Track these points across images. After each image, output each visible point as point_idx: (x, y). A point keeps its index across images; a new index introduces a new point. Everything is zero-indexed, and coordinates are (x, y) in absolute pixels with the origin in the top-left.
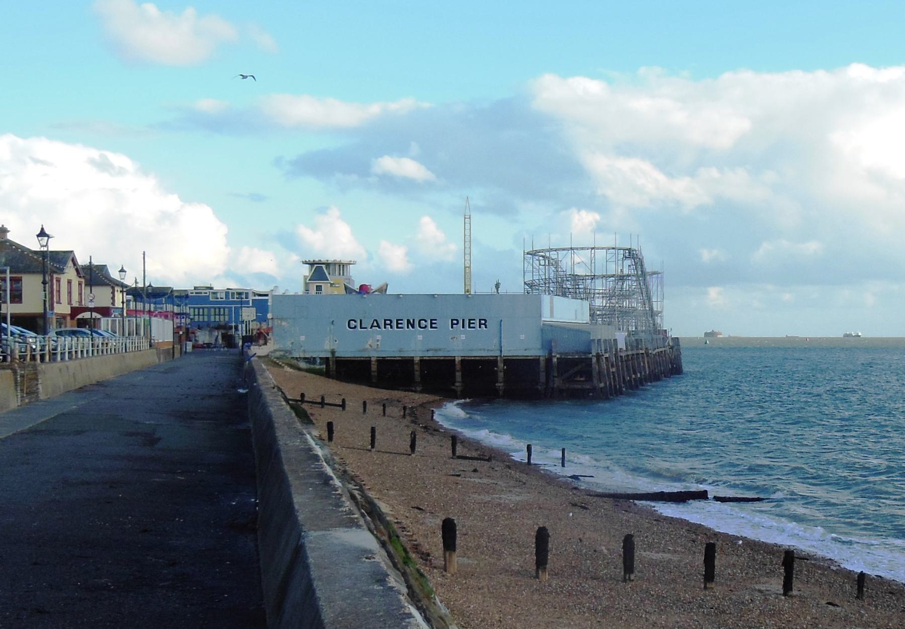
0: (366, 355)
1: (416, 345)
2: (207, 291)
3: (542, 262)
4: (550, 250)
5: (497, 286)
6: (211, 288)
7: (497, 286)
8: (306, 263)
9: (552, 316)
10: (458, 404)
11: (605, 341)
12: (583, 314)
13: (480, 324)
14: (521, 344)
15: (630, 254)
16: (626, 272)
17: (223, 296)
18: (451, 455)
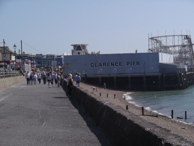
0: (97, 76)
1: (115, 72)
2: (40, 56)
3: (155, 42)
4: (158, 37)
5: (136, 52)
6: (42, 55)
7: (136, 52)
8: (72, 45)
9: (162, 60)
10: (129, 95)
11: (182, 69)
12: (171, 59)
13: (137, 64)
14: (152, 71)
15: (187, 37)
16: (185, 44)
17: (46, 57)
18: (141, 114)
